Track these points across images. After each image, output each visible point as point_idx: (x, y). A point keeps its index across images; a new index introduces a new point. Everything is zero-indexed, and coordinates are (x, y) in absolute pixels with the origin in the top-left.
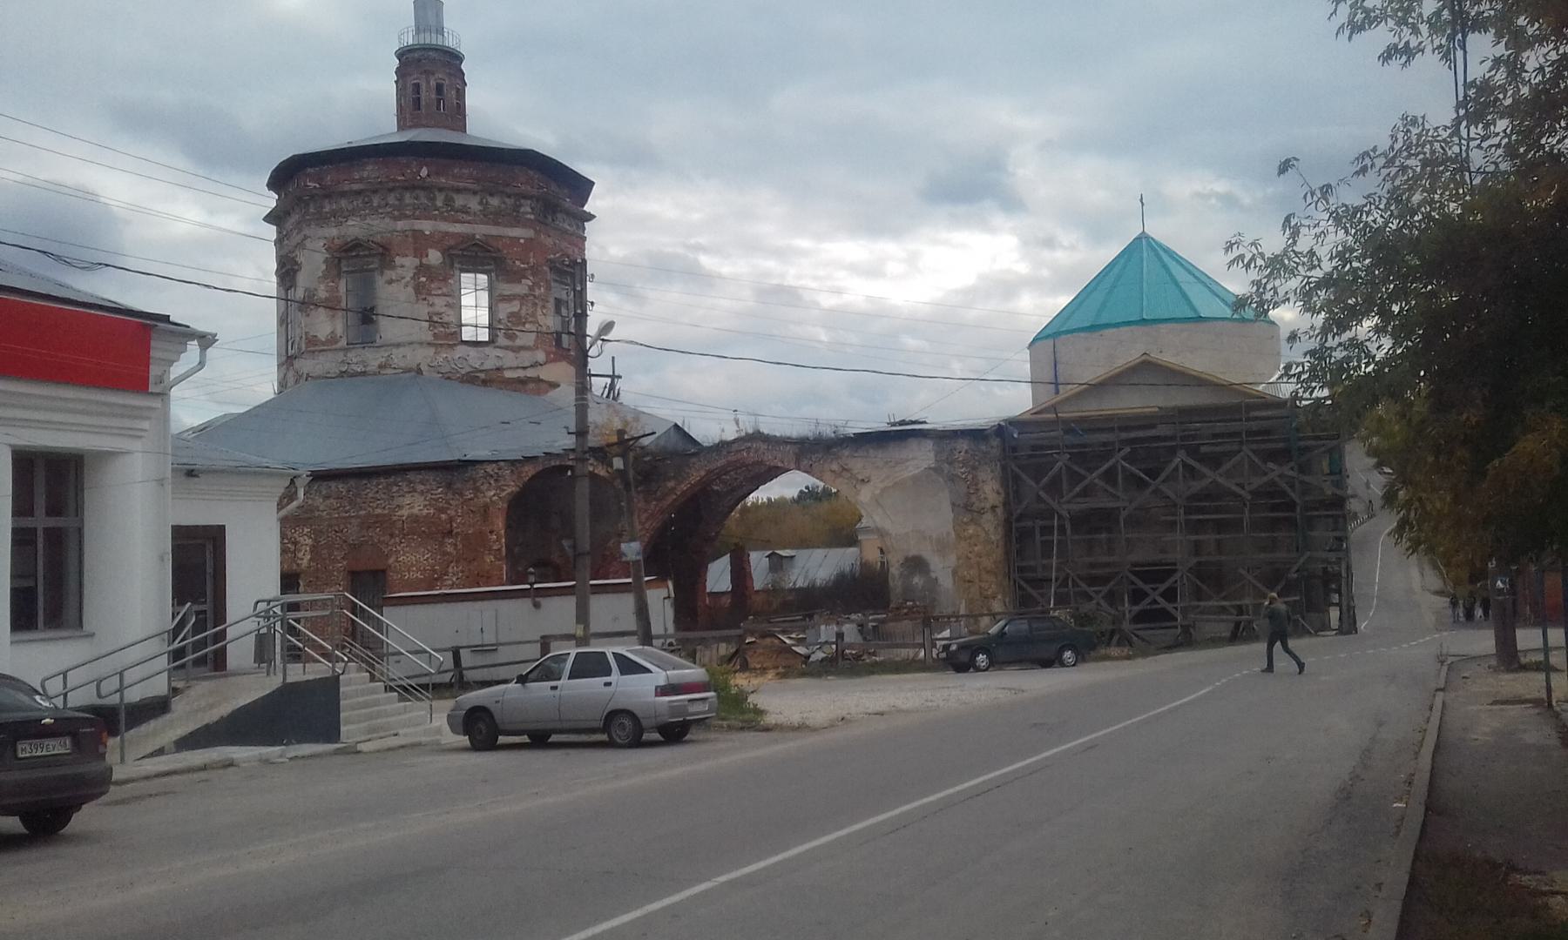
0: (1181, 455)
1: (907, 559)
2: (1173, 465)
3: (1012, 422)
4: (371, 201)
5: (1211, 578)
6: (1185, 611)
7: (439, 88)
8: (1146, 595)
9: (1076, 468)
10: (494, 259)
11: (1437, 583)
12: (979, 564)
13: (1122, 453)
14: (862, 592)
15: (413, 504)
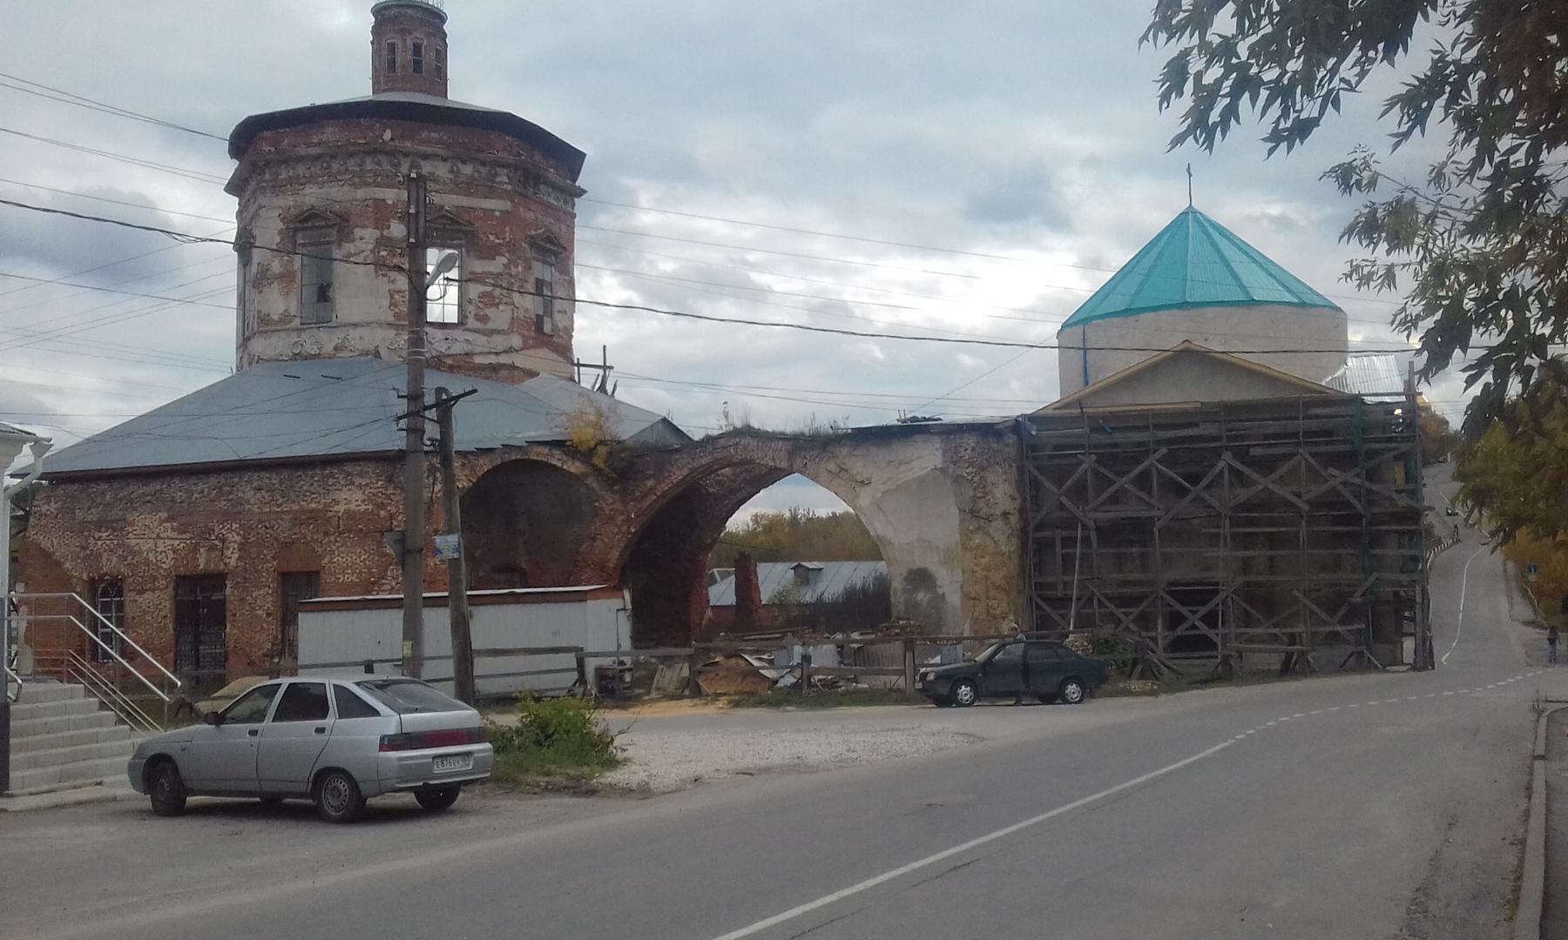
0: (1227, 457)
1: (911, 572)
2: (1217, 469)
3: (1032, 418)
4: (329, 167)
5: (1262, 602)
6: (1225, 637)
7: (417, 49)
8: (1184, 619)
9: (1102, 470)
10: (466, 233)
11: (1528, 614)
12: (986, 578)
13: (1158, 455)
14: (867, 609)
15: (350, 498)
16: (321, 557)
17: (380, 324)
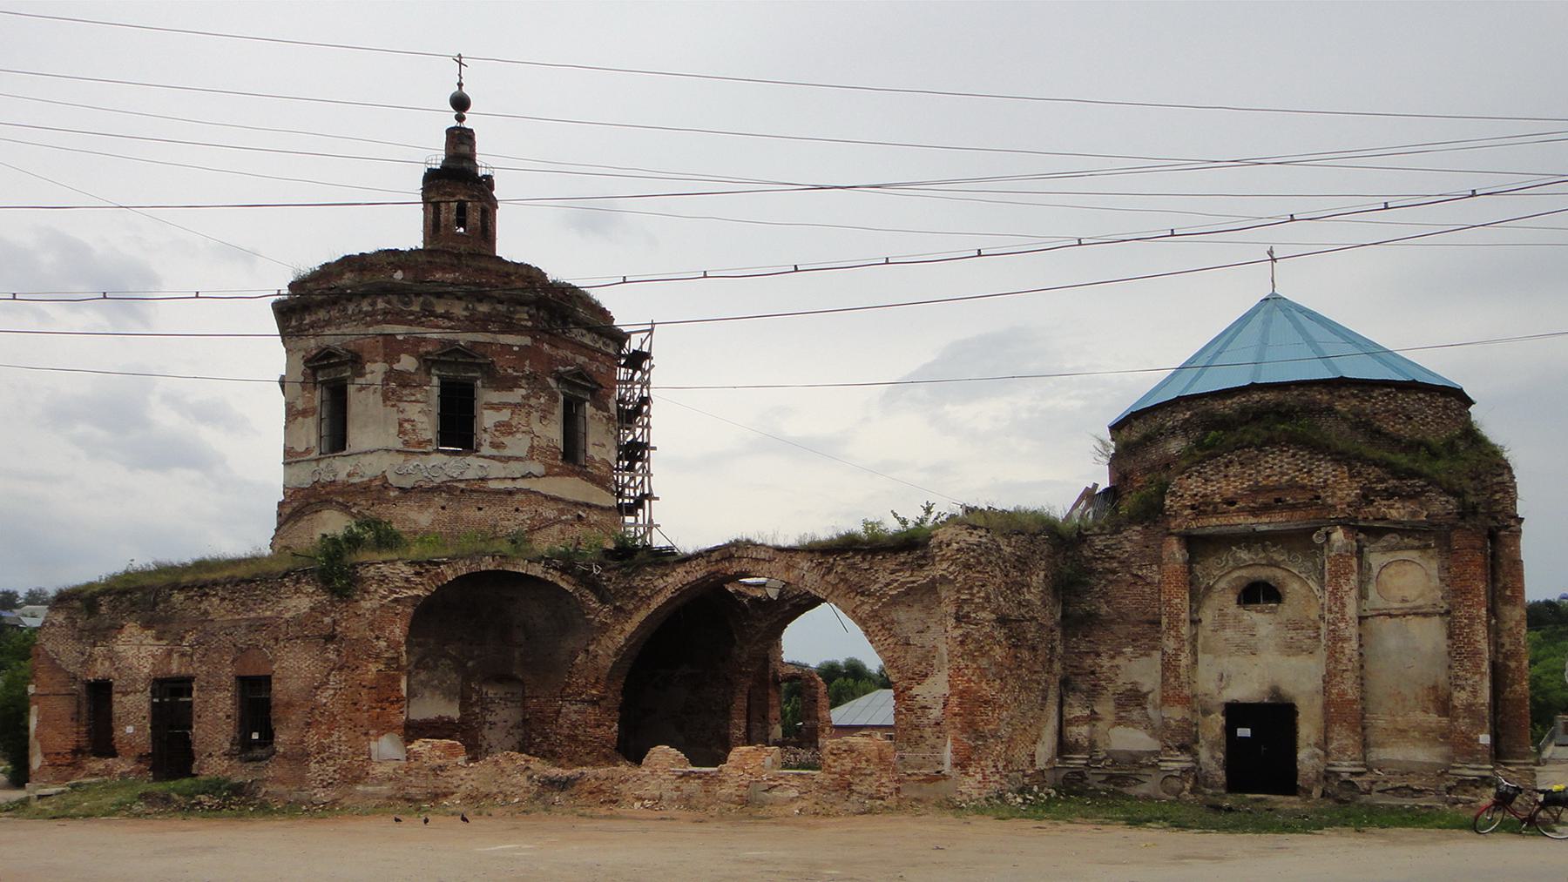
4: (345, 309)
16: (272, 662)
17: (388, 451)
